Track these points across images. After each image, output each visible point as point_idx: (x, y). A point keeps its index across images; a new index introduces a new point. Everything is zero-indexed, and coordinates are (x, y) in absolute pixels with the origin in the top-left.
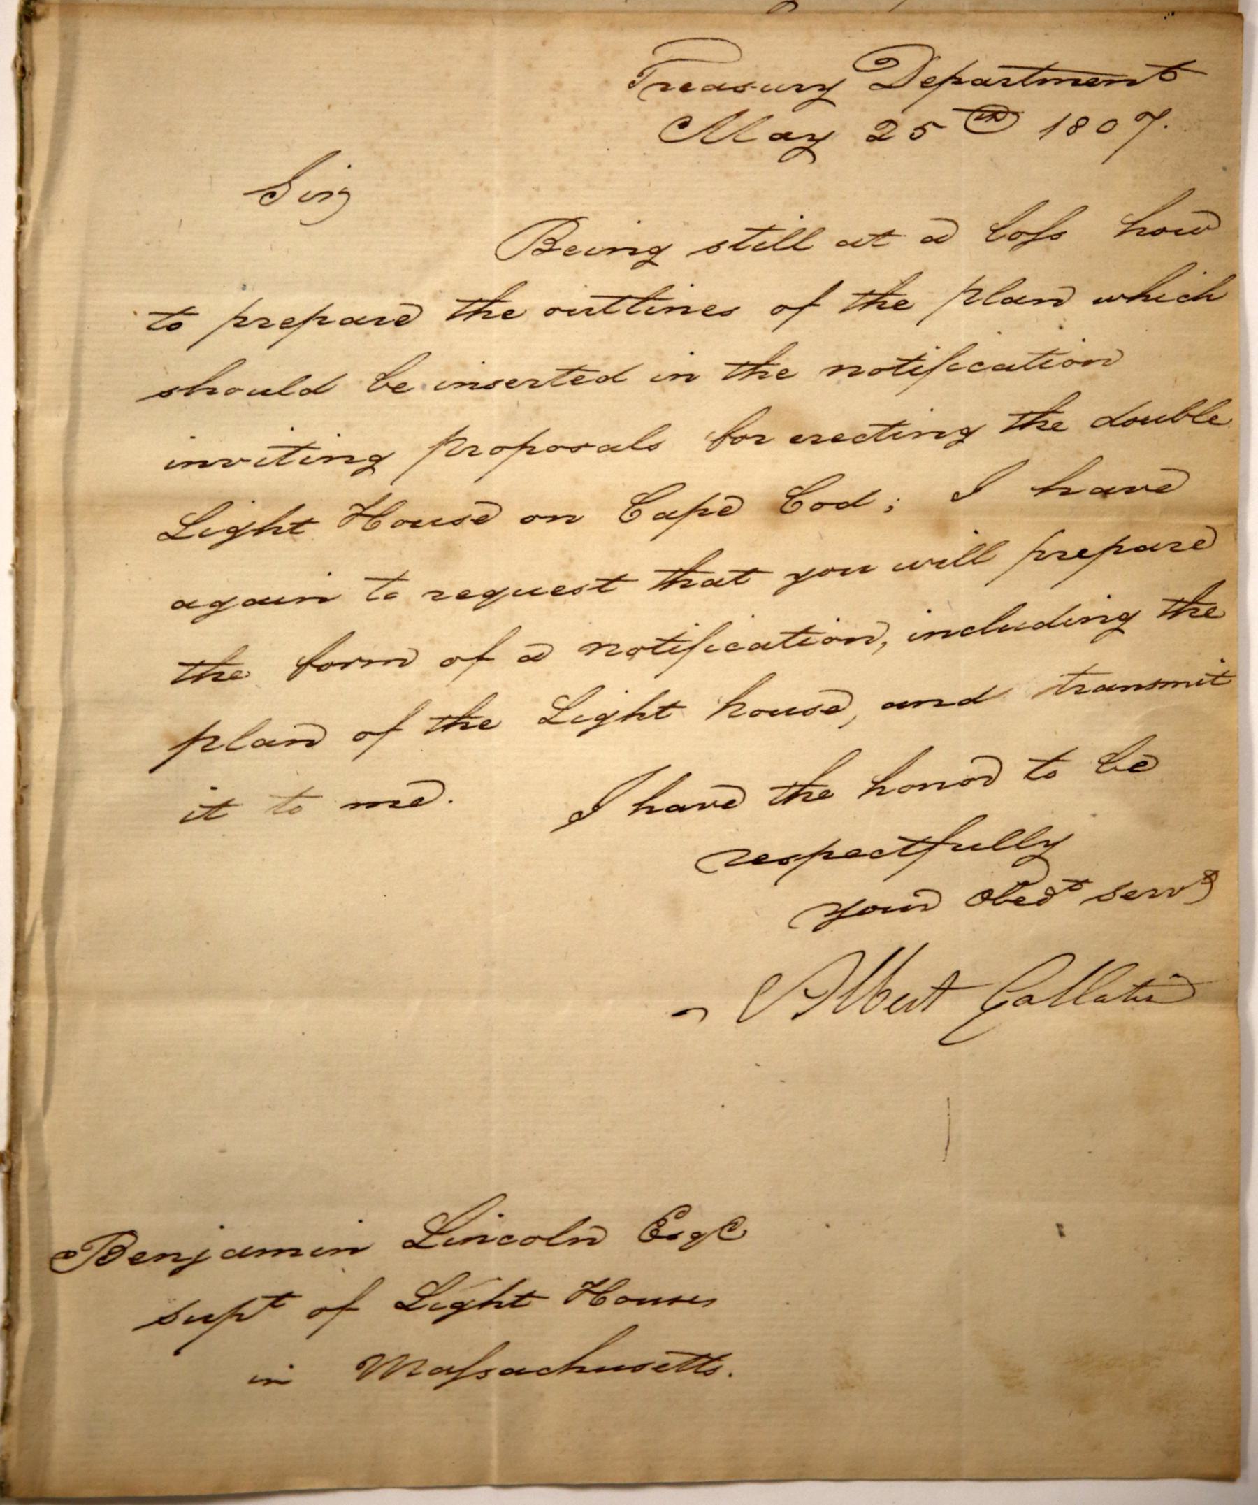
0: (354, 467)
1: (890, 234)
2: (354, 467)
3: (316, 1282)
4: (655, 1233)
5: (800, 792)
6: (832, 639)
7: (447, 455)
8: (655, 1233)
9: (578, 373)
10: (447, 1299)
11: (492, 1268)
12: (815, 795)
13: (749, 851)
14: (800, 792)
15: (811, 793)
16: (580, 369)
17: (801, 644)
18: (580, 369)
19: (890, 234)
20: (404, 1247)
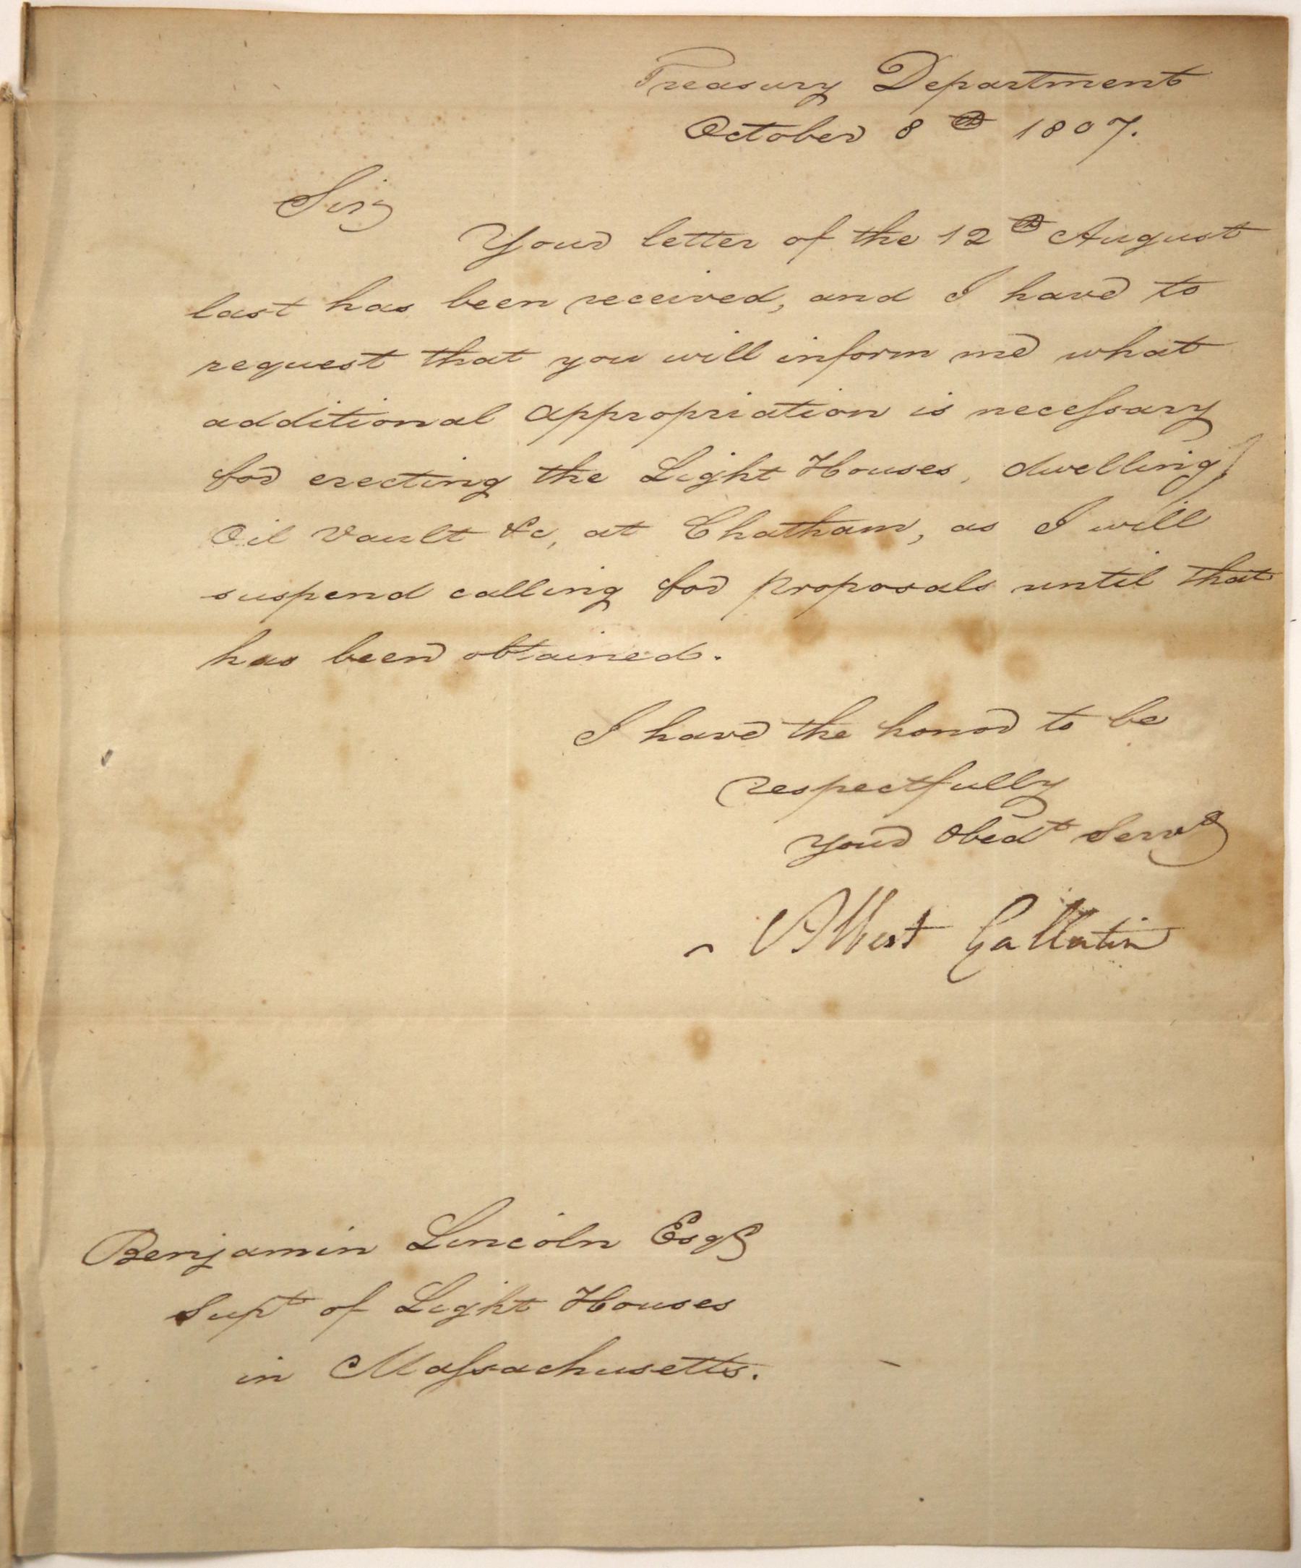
0: (685, 485)
1: (466, 531)
2: (685, 485)
3: (331, 1279)
4: (670, 1235)
5: (814, 730)
6: (837, 411)
7: (545, 594)
8: (670, 1235)
9: (805, 409)
10: (451, 1302)
11: (498, 1272)
12: (831, 734)
13: (769, 779)
14: (814, 730)
15: (827, 732)
16: (806, 404)
17: (707, 1371)
18: (806, 404)
19: (466, 531)
20: (358, 1357)
